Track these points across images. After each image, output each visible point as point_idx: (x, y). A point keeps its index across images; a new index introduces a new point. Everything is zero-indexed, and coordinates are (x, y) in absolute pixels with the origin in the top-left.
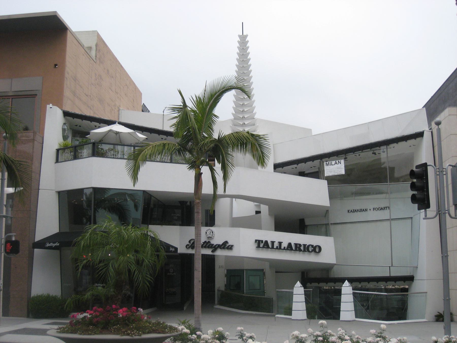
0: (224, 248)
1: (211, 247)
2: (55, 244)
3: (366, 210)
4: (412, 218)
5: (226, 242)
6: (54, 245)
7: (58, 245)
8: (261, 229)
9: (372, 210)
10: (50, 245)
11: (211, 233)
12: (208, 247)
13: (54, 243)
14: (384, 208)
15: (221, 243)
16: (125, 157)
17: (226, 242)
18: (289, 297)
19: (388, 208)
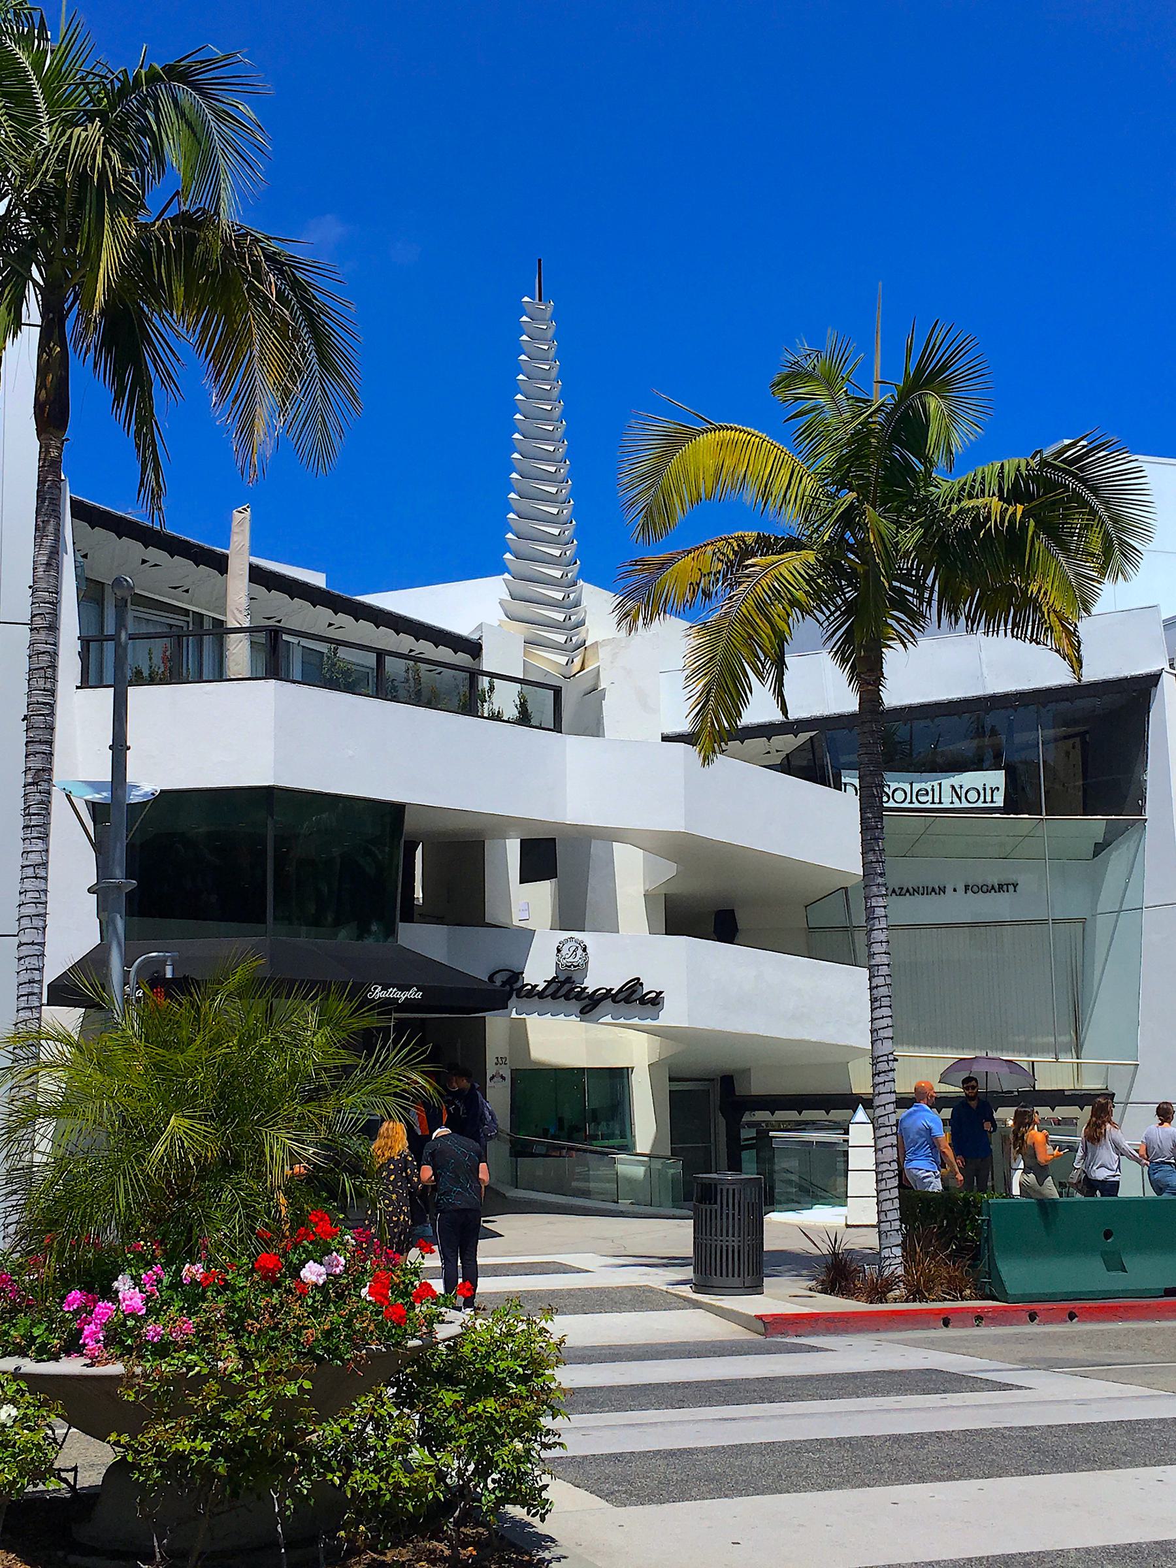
0: (627, 1000)
1: (578, 997)
2: (407, 994)
3: (943, 890)
4: (1083, 921)
5: (637, 983)
6: (402, 996)
7: (419, 995)
8: (731, 941)
9: (961, 888)
10: (384, 994)
11: (580, 952)
12: (567, 997)
13: (403, 988)
14: (1001, 886)
15: (616, 984)
16: (486, 679)
17: (637, 983)
18: (838, 1157)
19: (1011, 888)
